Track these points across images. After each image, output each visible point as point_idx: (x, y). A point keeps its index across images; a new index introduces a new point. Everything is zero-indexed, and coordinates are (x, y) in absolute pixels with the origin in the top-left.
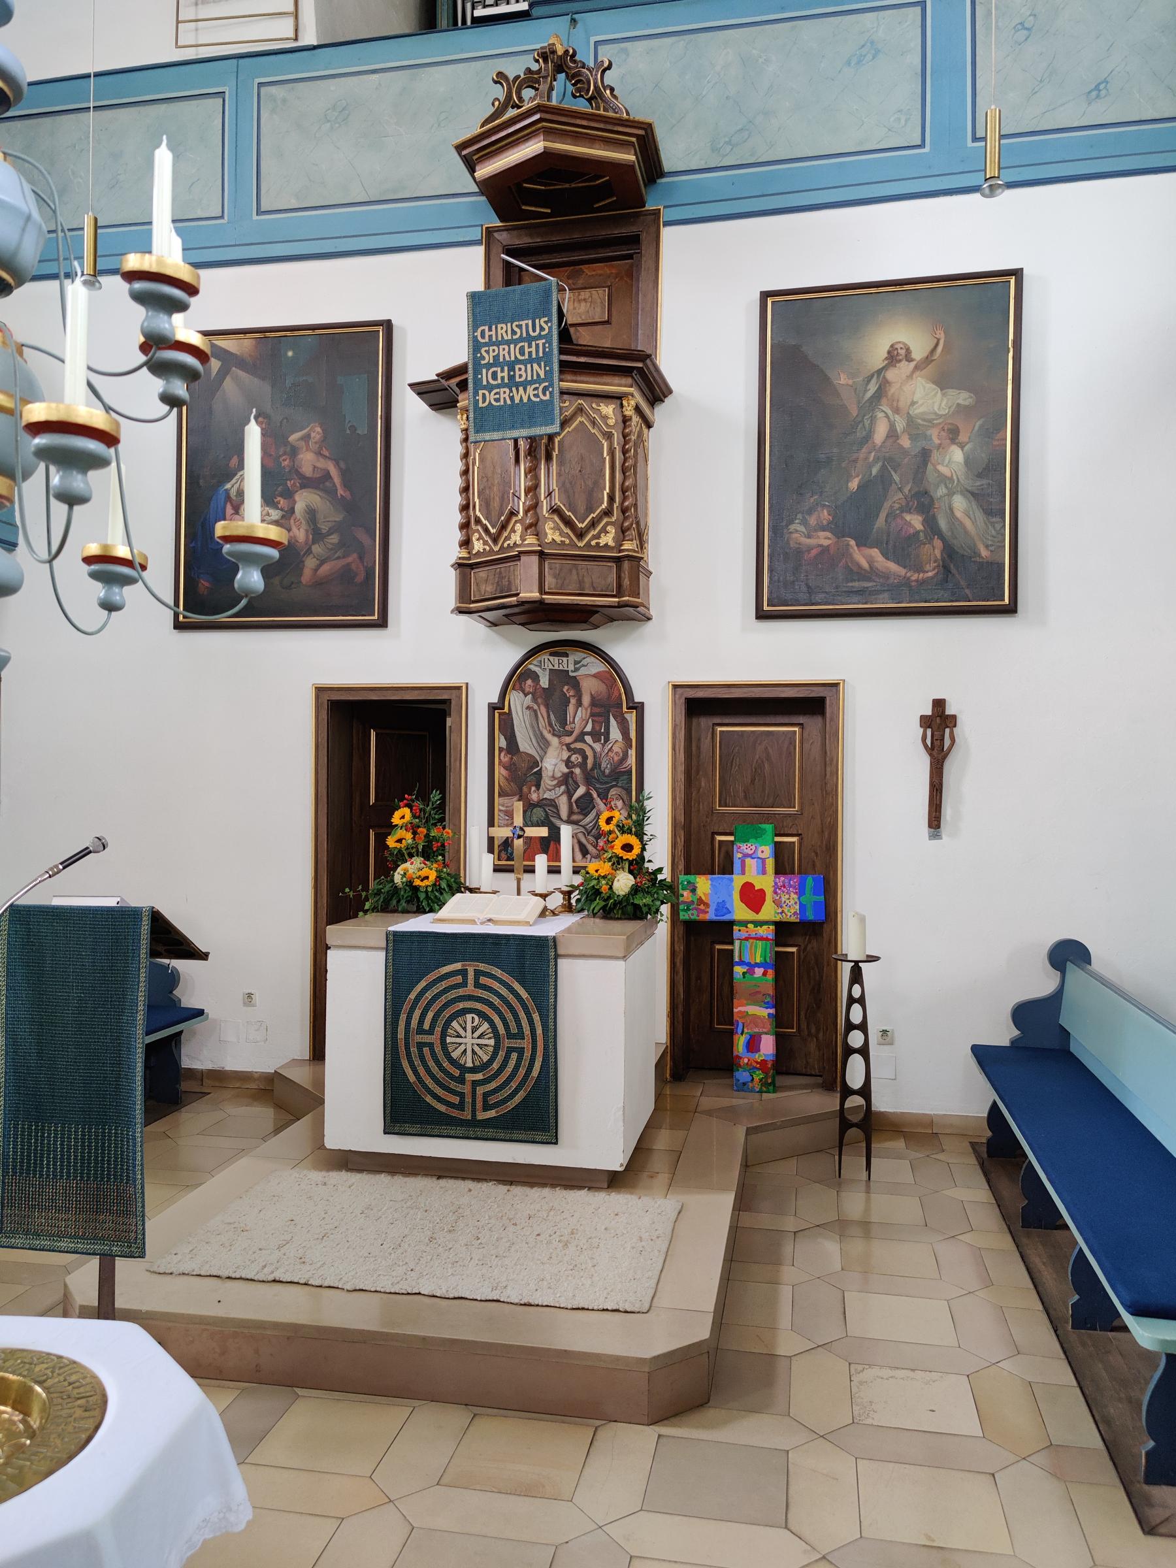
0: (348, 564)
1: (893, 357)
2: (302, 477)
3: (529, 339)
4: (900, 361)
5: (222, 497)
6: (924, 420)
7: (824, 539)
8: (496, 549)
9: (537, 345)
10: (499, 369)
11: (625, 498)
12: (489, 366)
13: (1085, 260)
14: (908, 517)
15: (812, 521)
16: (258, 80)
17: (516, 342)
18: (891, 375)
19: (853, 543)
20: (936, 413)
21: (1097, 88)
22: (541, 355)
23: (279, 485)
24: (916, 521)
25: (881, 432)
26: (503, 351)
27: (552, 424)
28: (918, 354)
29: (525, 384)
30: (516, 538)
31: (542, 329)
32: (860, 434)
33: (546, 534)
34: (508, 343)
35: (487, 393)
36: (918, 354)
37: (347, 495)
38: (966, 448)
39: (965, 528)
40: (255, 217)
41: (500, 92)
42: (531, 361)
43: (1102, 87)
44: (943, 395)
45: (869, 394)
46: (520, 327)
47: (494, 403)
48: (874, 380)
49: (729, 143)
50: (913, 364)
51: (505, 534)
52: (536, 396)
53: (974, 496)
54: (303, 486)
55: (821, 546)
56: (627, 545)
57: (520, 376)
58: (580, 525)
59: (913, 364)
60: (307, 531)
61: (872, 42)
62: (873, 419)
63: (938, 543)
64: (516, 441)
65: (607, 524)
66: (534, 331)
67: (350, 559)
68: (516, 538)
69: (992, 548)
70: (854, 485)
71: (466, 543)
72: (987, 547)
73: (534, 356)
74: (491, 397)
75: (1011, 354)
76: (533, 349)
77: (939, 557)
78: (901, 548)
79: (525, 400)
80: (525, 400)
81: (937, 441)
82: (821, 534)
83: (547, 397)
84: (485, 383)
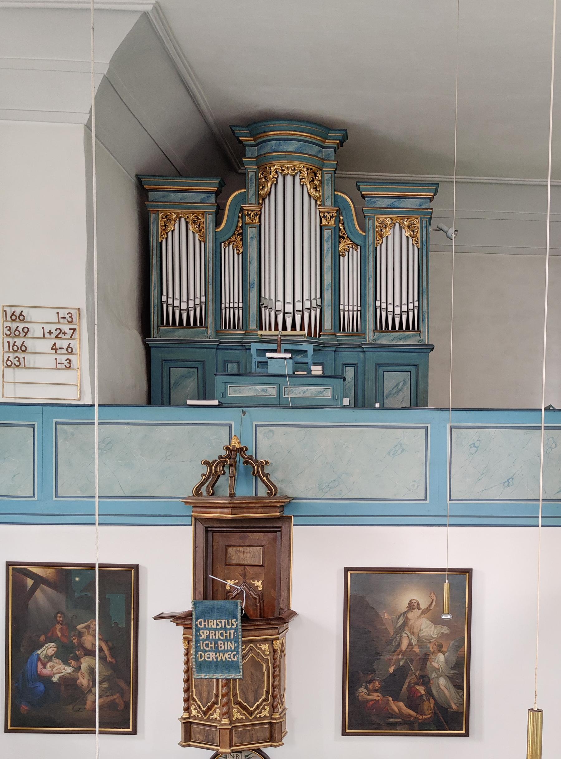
0: (114, 699)
1: (411, 607)
2: (84, 649)
3: (226, 629)
4: (414, 609)
5: (35, 658)
6: (427, 640)
7: (376, 696)
8: (205, 718)
9: (230, 633)
10: (209, 643)
11: (274, 691)
12: (204, 640)
13: (504, 566)
14: (418, 687)
15: (370, 686)
16: (55, 420)
17: (219, 630)
18: (410, 615)
19: (390, 699)
20: (431, 636)
21: (508, 481)
22: (232, 638)
23: (72, 653)
24: (421, 689)
25: (404, 645)
26: (212, 634)
27: (238, 673)
28: (423, 606)
29: (224, 652)
30: (216, 716)
31: (233, 625)
32: (395, 644)
33: (233, 716)
34: (215, 630)
35: (203, 654)
36: (423, 606)
37: (113, 660)
38: (446, 654)
39: (444, 694)
40: (55, 499)
41: (205, 470)
42: (226, 640)
43: (510, 481)
44: (435, 627)
45: (399, 624)
46: (221, 622)
47: (207, 659)
48: (402, 617)
49: (328, 486)
50: (421, 611)
51: (210, 712)
52: (230, 658)
53: (451, 679)
54: (86, 655)
55: (375, 700)
56: (276, 716)
57: (221, 647)
58: (251, 709)
59: (421, 611)
60: (89, 680)
61: (401, 444)
62: (401, 638)
63: (432, 701)
64: (217, 680)
65: (265, 705)
66: (229, 625)
67: (115, 697)
68: (216, 716)
69: (458, 705)
70: (391, 670)
71: (187, 709)
72: (455, 704)
73: (228, 638)
74: (205, 656)
75: (467, 611)
76: (228, 634)
77: (432, 708)
78: (414, 702)
79: (224, 660)
80: (224, 660)
81: (432, 650)
82: (376, 694)
83: (236, 659)
84: (202, 648)
